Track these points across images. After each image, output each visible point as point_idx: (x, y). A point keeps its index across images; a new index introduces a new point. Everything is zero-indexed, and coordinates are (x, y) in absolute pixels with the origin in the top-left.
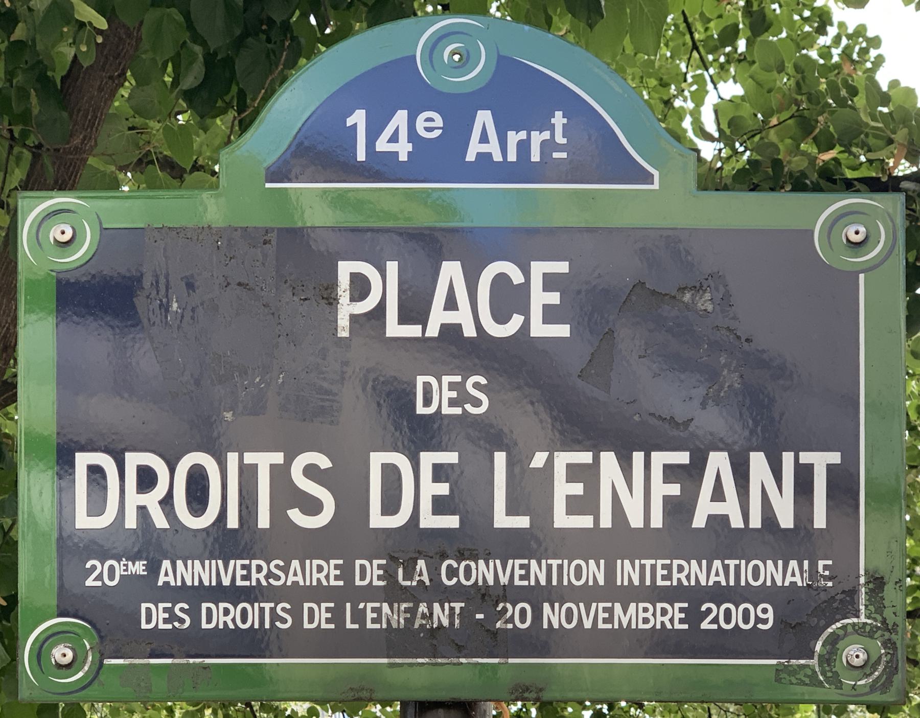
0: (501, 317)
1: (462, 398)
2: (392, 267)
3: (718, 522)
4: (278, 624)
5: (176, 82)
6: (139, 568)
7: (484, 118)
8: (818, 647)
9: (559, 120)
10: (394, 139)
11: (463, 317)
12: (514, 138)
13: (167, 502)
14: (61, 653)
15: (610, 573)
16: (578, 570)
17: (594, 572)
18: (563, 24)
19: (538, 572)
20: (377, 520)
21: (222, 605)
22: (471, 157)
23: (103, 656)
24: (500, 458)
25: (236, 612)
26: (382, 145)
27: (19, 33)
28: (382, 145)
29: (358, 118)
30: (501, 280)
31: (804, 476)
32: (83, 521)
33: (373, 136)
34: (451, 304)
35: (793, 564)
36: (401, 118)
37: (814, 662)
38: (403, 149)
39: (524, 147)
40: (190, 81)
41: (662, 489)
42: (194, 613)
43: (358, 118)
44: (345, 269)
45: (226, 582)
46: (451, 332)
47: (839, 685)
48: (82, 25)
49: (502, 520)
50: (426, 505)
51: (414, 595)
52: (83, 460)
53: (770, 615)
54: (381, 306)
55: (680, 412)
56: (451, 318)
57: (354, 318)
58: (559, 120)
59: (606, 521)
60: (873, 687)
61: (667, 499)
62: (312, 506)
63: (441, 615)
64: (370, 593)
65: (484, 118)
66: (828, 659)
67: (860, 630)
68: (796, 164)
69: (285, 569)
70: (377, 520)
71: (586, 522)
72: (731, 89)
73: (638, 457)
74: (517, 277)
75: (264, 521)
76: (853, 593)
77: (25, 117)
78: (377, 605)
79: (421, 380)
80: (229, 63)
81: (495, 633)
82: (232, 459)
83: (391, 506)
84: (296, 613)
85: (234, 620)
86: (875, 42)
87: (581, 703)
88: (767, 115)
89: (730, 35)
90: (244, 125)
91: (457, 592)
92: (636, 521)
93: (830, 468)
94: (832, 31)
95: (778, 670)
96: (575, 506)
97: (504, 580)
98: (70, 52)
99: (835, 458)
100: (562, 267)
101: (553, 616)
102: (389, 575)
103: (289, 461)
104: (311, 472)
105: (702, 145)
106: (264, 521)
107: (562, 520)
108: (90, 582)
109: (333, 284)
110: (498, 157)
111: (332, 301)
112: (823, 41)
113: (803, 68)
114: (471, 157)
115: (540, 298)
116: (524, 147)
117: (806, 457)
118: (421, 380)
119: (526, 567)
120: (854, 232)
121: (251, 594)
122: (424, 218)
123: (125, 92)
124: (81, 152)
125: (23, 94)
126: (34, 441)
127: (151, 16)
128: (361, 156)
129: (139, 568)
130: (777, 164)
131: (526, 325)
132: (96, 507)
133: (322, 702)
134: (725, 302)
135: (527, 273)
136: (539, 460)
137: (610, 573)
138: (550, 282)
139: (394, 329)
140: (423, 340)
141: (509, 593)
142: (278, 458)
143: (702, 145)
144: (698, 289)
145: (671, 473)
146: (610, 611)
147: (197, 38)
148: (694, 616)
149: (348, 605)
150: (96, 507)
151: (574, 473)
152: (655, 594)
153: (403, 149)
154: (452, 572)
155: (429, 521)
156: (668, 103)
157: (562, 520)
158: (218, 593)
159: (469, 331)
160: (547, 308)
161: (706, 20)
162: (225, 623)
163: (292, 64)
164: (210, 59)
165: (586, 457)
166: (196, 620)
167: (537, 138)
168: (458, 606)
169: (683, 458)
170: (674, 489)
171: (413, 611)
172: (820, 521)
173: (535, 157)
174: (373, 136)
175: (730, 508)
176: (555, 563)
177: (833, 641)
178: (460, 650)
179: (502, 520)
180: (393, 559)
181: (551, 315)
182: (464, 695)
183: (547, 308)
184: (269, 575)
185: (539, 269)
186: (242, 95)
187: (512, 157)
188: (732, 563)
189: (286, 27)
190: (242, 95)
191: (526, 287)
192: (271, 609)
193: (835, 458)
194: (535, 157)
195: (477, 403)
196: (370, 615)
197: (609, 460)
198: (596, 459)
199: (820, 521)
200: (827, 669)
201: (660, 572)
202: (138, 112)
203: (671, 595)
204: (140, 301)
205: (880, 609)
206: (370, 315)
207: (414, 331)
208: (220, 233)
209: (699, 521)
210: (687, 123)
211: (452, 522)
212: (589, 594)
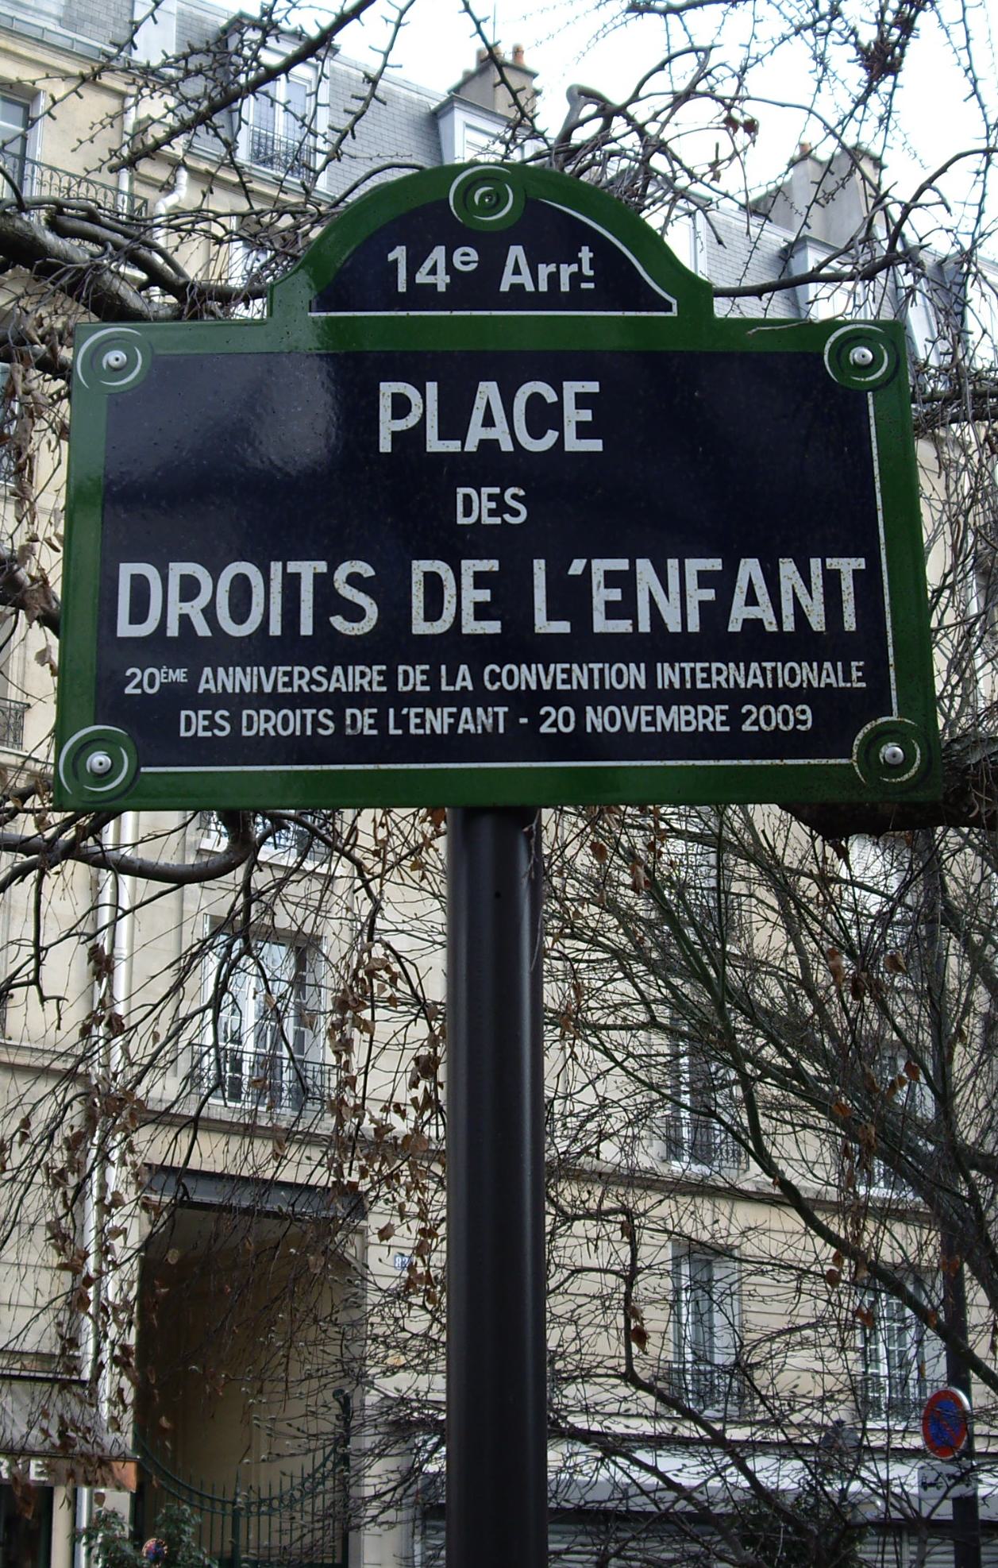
1: (501, 508)
4: (338, 622)
9: (586, 254)
12: (544, 270)
13: (209, 612)
17: (635, 675)
20: (420, 626)
26: (422, 278)
38: (442, 281)
39: (554, 279)
42: (235, 720)
49: (543, 625)
74: (551, 396)
103: (332, 568)
115: (573, 415)
128: (402, 287)
154: (495, 677)
157: (601, 624)
159: (507, 446)
167: (566, 271)
173: (565, 287)
179: (543, 625)
192: (317, 576)
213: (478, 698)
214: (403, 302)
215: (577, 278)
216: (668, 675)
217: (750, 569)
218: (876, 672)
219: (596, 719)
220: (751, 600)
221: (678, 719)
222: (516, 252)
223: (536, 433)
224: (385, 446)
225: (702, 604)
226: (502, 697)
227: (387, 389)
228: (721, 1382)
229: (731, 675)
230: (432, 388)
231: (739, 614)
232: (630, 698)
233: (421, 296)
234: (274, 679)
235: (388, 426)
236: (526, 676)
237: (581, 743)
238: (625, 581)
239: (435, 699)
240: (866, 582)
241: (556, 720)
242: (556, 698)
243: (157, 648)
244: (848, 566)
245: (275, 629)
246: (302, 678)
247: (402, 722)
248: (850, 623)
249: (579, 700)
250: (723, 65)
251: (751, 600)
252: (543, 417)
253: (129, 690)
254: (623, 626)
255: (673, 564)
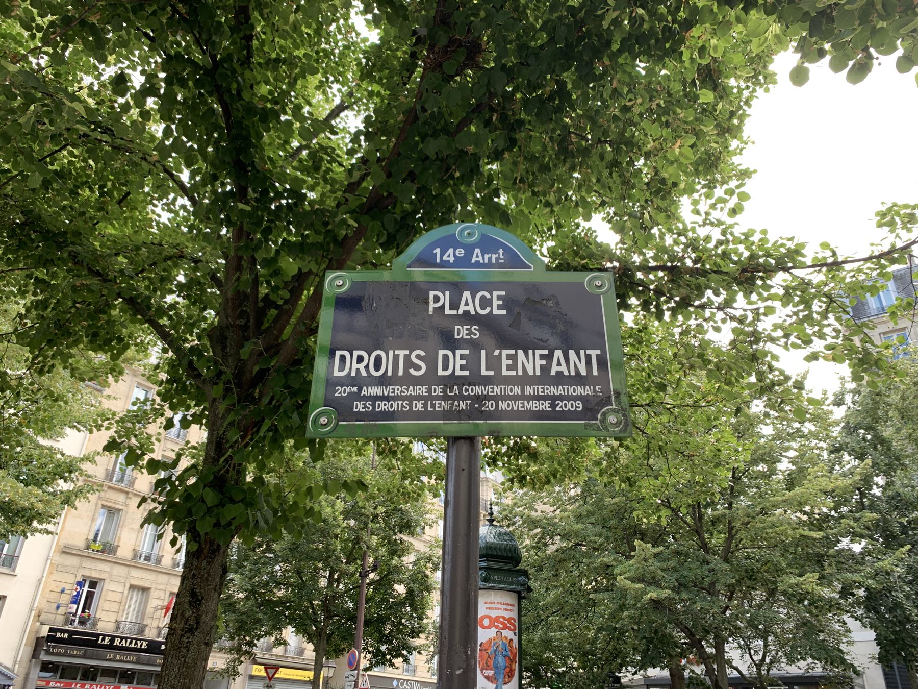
0: (483, 308)
1: (470, 333)
2: (447, 293)
3: (559, 373)
5: (377, 241)
6: (355, 389)
7: (477, 251)
8: (599, 416)
9: (501, 251)
10: (449, 256)
11: (470, 308)
12: (487, 256)
13: (367, 367)
14: (323, 420)
15: (523, 390)
16: (511, 389)
17: (517, 390)
18: (499, 225)
19: (497, 390)
20: (441, 373)
22: (473, 261)
23: (338, 421)
24: (483, 352)
25: (389, 405)
26: (445, 258)
27: (330, 227)
28: (445, 258)
30: (483, 297)
31: (588, 359)
32: (336, 373)
34: (467, 304)
35: (587, 387)
36: (451, 251)
37: (598, 422)
38: (452, 259)
39: (490, 259)
40: (382, 241)
41: (539, 362)
42: (373, 405)
43: (438, 251)
44: (432, 294)
45: (386, 394)
46: (467, 313)
47: (608, 430)
48: (349, 225)
49: (484, 372)
50: (458, 367)
51: (453, 398)
52: (338, 353)
53: (581, 405)
54: (444, 305)
55: (544, 337)
56: (467, 308)
57: (434, 309)
58: (501, 251)
59: (520, 373)
60: (620, 431)
61: (541, 366)
62: (418, 368)
63: (462, 405)
64: (437, 398)
65: (477, 251)
66: (603, 421)
67: (613, 410)
68: (574, 264)
69: (407, 390)
70: (441, 373)
71: (513, 373)
72: (551, 244)
73: (530, 352)
74: (488, 296)
75: (401, 373)
76: (610, 397)
77: (328, 250)
79: (456, 327)
80: (394, 236)
81: (482, 412)
82: (391, 352)
83: (446, 367)
84: (410, 405)
86: (595, 231)
87: (509, 437)
88: (563, 251)
89: (550, 229)
90: (399, 253)
91: (468, 397)
92: (531, 373)
93: (597, 355)
94: (581, 228)
95: (585, 425)
96: (509, 368)
97: (485, 393)
98: (344, 233)
99: (599, 352)
100: (503, 293)
101: (503, 405)
102: (444, 391)
103: (410, 353)
104: (418, 357)
105: (543, 258)
106: (401, 373)
107: (505, 372)
108: (336, 395)
109: (428, 298)
110: (482, 261)
111: (427, 303)
112: (578, 231)
113: (574, 238)
114: (473, 261)
115: (496, 302)
116: (490, 259)
117: (588, 352)
118: (456, 327)
119: (493, 389)
120: (598, 283)
121: (395, 398)
122: (456, 279)
123: (361, 244)
124: (345, 261)
125: (328, 244)
126: (321, 348)
127: (371, 223)
128: (438, 261)
129: (355, 389)
130: (568, 264)
131: (491, 311)
132: (341, 369)
133: (414, 438)
134: (557, 303)
135: (491, 295)
137: (523, 390)
138: (499, 298)
139: (447, 311)
140: (457, 315)
141: (487, 397)
143: (543, 258)
144: (548, 300)
145: (542, 357)
146: (523, 404)
147: (385, 229)
148: (553, 406)
150: (341, 369)
151: (509, 357)
152: (538, 398)
153: (452, 259)
154: (467, 390)
155: (458, 373)
156: (531, 247)
157: (505, 372)
158: (383, 398)
159: (473, 312)
160: (498, 306)
161: (542, 225)
163: (414, 236)
164: (389, 235)
165: (513, 352)
166: (374, 407)
167: (494, 256)
168: (469, 402)
169: (546, 352)
170: (544, 362)
171: (452, 404)
172: (595, 373)
173: (494, 261)
174: (442, 255)
175: (563, 368)
176: (503, 387)
177: (604, 414)
178: (470, 418)
179: (484, 372)
180: (446, 386)
182: (471, 434)
183: (498, 306)
184: (402, 391)
185: (495, 294)
186: (398, 245)
187: (486, 261)
188: (566, 387)
189: (413, 226)
190: (398, 245)
191: (491, 298)
193: (599, 352)
194: (494, 261)
195: (475, 334)
196: (437, 405)
197: (520, 353)
198: (516, 352)
199: (595, 373)
200: (779, 426)
201: (540, 390)
202: (365, 249)
203: (544, 398)
204: (363, 303)
205: (620, 403)
206: (439, 308)
207: (454, 312)
208: (391, 283)
209: (553, 373)
210: (538, 253)
211: (467, 373)
212: (515, 398)
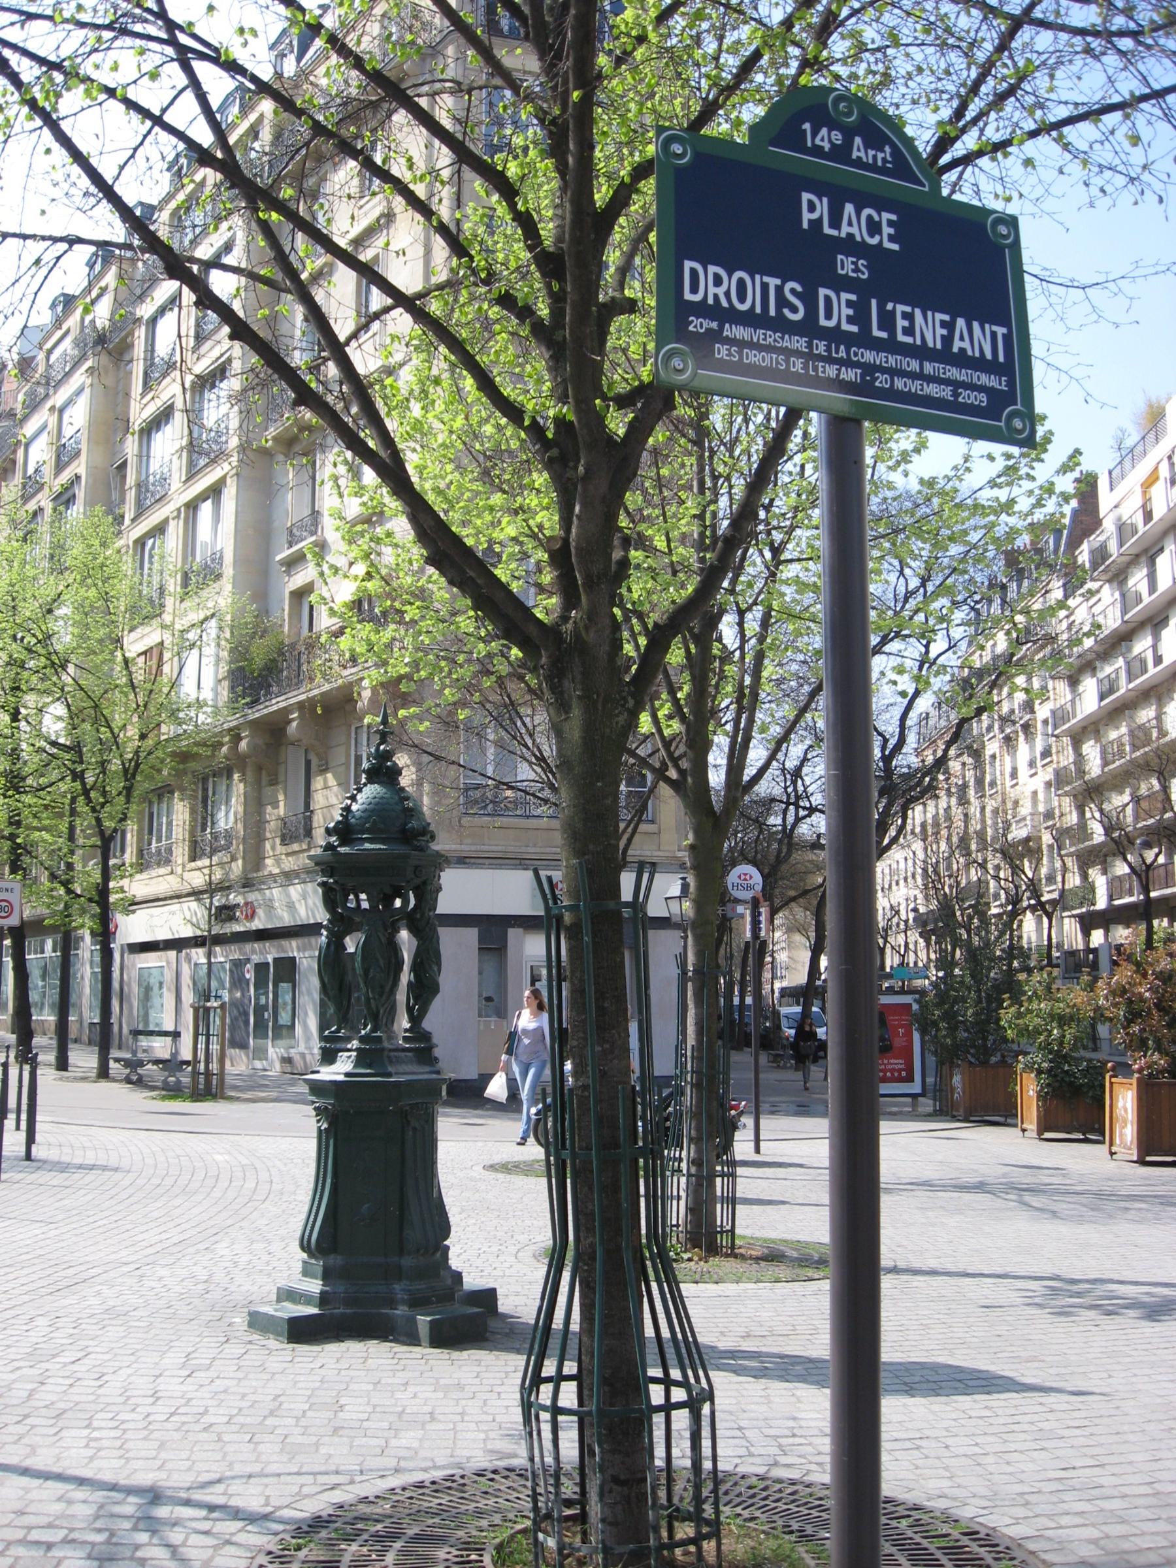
1: (857, 270)
4: (786, 311)
6: (714, 325)
9: (887, 149)
11: (854, 230)
12: (871, 153)
13: (727, 294)
17: (914, 365)
20: (823, 322)
21: (712, 269)
26: (818, 142)
29: (807, 126)
30: (870, 217)
33: (814, 135)
38: (827, 146)
39: (875, 157)
42: (740, 353)
49: (876, 333)
74: (876, 218)
78: (908, 309)
85: (727, 294)
103: (783, 283)
115: (887, 230)
128: (809, 144)
129: (714, 325)
136: (890, 306)
142: (778, 282)
145: (943, 324)
149: (874, 302)
151: (905, 316)
154: (856, 354)
157: (901, 338)
159: (858, 239)
162: (716, 296)
167: (880, 155)
173: (880, 163)
174: (814, 135)
179: (876, 333)
181: (891, 238)
191: (880, 223)
192: (777, 287)
196: (901, 323)
213: (848, 363)
214: (803, 149)
215: (884, 160)
216: (929, 368)
217: (961, 323)
218: (1011, 383)
219: (899, 384)
220: (962, 339)
221: (933, 390)
222: (858, 140)
223: (872, 236)
224: (805, 225)
225: (942, 336)
226: (857, 365)
227: (806, 196)
228: (1007, 613)
229: (954, 373)
230: (825, 200)
231: (957, 345)
232: (913, 376)
233: (817, 151)
234: (759, 335)
235: (806, 216)
236: (869, 356)
237: (740, 369)
238: (908, 316)
239: (830, 360)
240: (1007, 338)
241: (882, 381)
242: (884, 370)
243: (701, 309)
244: (1001, 331)
245: (758, 310)
246: (771, 338)
247: (816, 369)
248: (1001, 359)
249: (894, 372)
250: (1110, 473)
251: (962, 339)
252: (874, 227)
253: (691, 328)
254: (909, 340)
255: (929, 314)
